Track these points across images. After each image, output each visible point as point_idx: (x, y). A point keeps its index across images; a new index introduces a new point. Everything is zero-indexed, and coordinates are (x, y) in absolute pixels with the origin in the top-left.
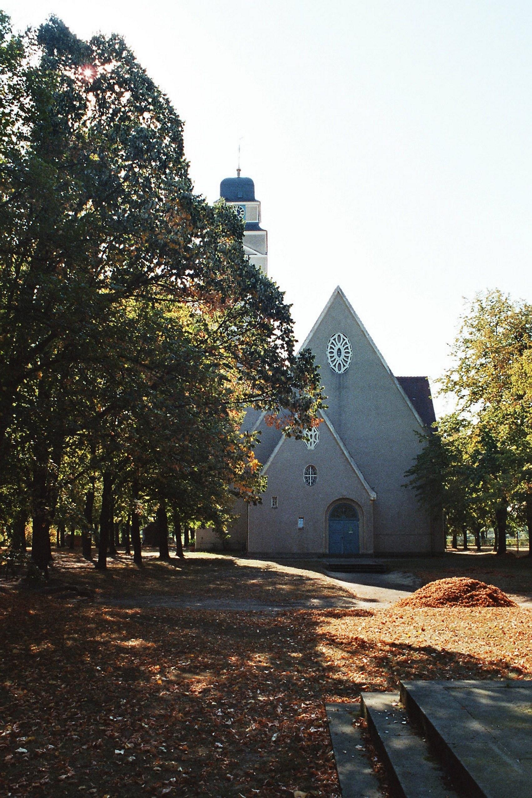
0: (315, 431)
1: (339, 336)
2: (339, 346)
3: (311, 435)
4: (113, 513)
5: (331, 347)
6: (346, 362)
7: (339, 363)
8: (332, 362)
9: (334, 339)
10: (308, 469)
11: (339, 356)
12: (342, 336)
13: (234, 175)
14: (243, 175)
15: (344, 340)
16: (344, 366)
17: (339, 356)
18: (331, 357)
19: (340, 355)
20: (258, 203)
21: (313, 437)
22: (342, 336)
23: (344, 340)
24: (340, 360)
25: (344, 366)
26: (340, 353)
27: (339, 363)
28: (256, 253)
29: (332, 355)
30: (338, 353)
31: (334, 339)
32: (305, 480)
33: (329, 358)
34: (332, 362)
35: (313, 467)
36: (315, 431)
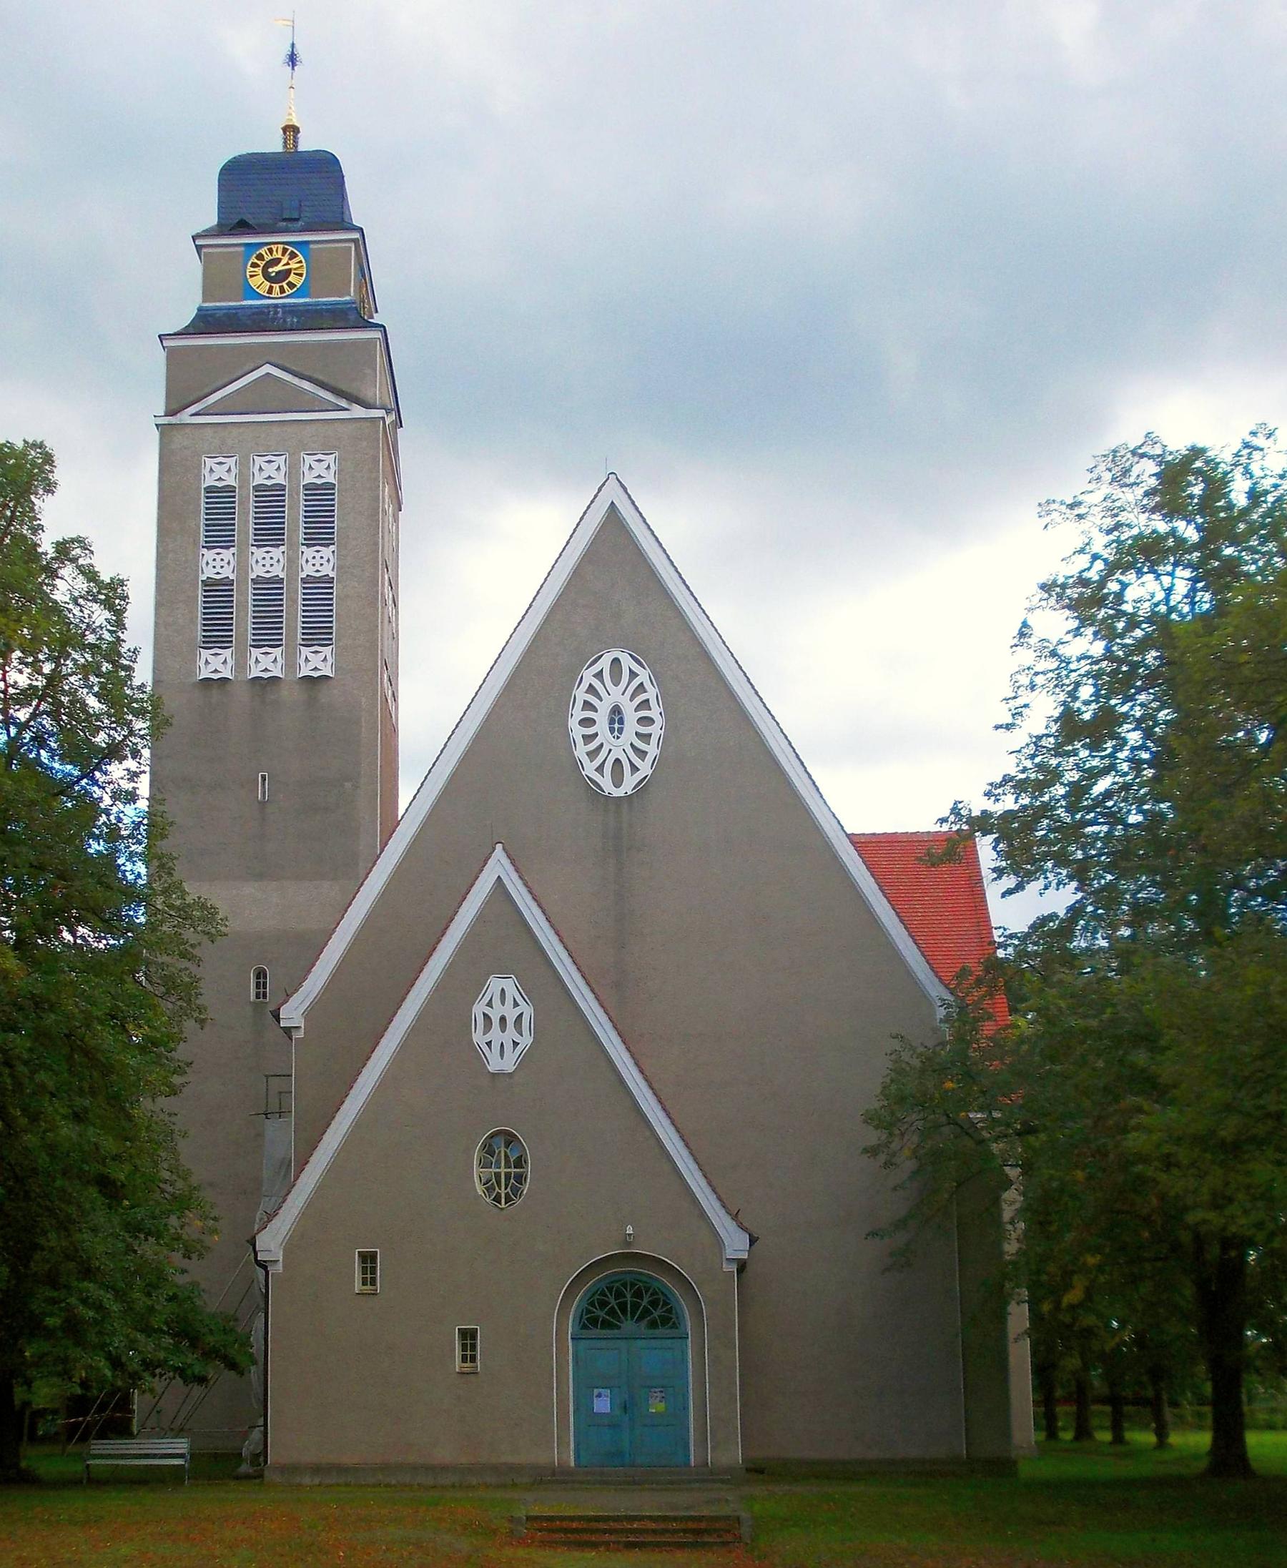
0: (516, 1004)
1: (616, 661)
2: (614, 695)
3: (503, 1019)
4: (1127, 838)
5: (585, 702)
6: (642, 754)
7: (617, 761)
8: (592, 755)
9: (599, 675)
10: (489, 1149)
11: (616, 711)
12: (627, 662)
13: (274, 145)
14: (307, 144)
15: (633, 675)
16: (634, 769)
17: (616, 711)
18: (588, 739)
19: (621, 731)
20: (356, 235)
21: (496, 1022)
22: (627, 662)
23: (633, 675)
24: (619, 747)
25: (634, 769)
26: (621, 721)
27: (617, 761)
28: (343, 403)
29: (590, 731)
30: (612, 722)
31: (599, 675)
32: (480, 1189)
33: (580, 741)
34: (592, 755)
35: (510, 1139)
36: (516, 1004)
